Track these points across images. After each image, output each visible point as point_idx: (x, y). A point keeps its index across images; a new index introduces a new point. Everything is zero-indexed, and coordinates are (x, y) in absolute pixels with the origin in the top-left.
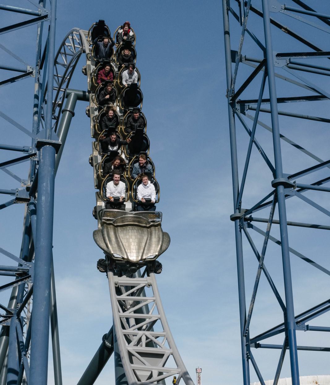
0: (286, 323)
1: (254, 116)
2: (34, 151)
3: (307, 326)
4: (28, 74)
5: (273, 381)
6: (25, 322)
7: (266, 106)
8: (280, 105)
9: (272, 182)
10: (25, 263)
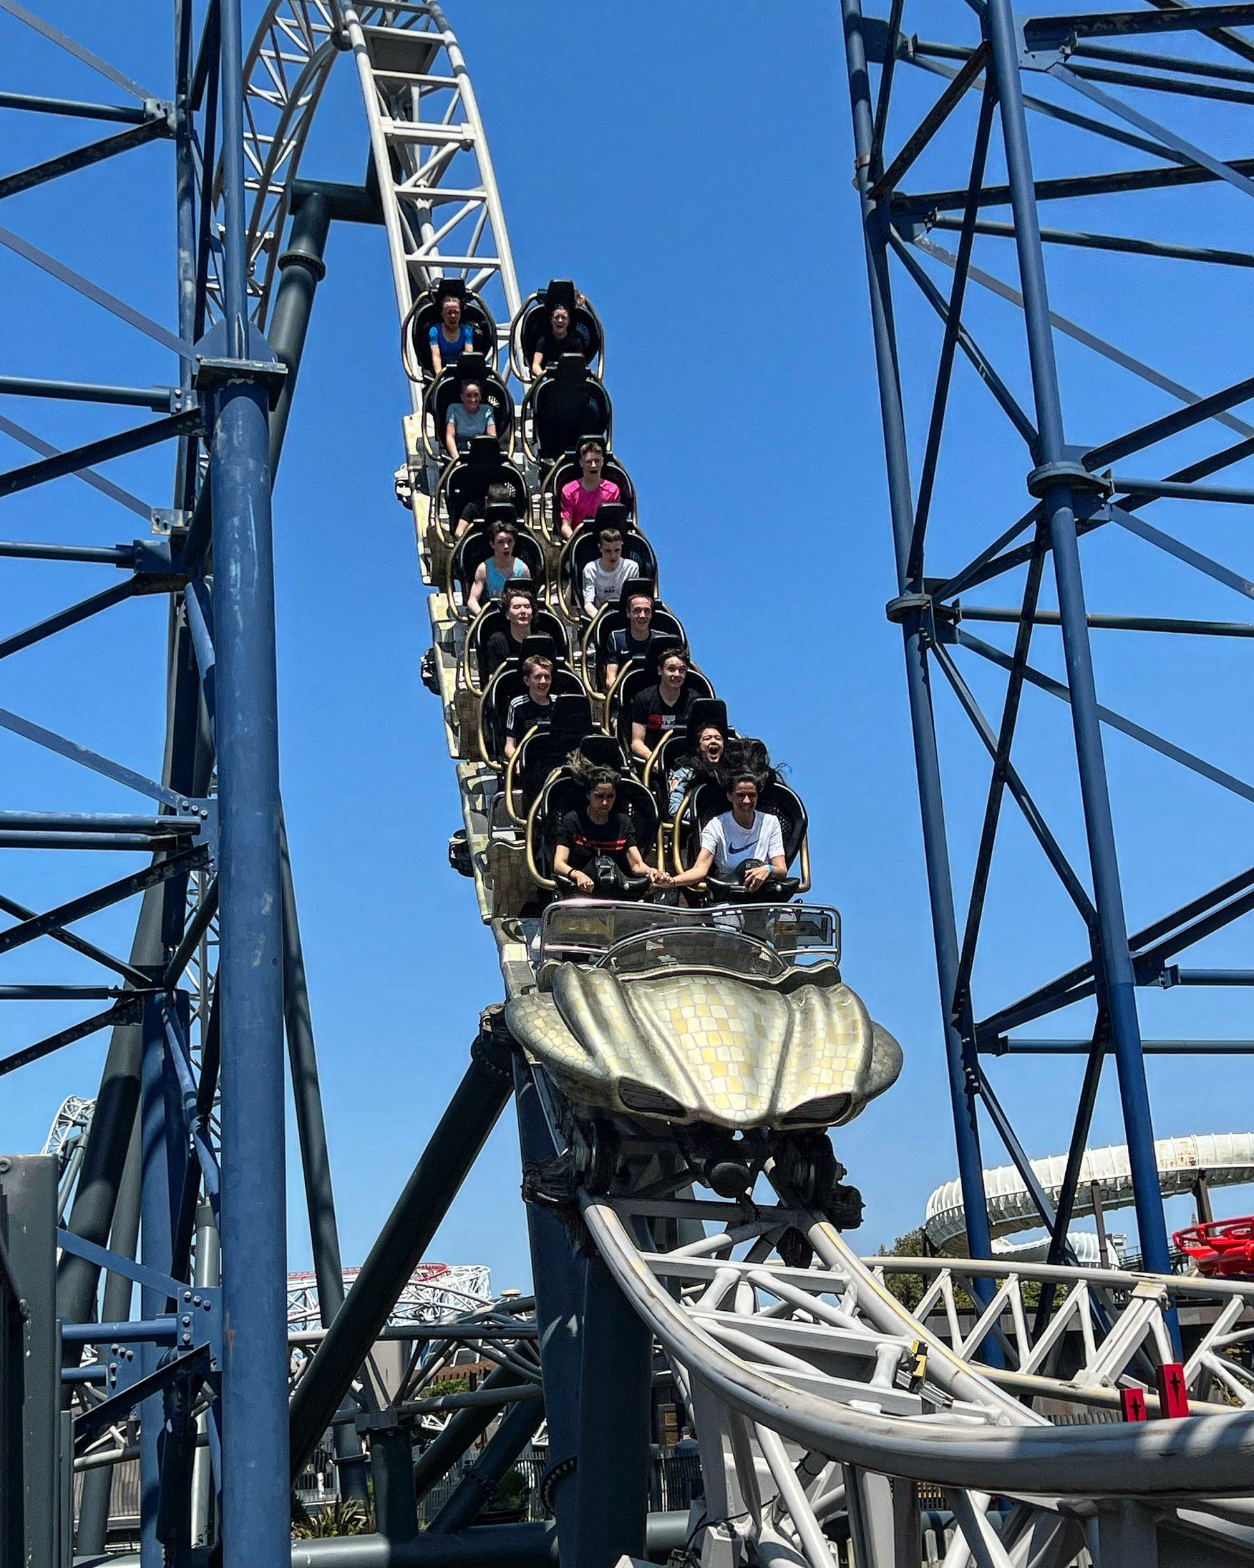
0: (1100, 964)
1: (954, 250)
2: (189, 402)
3: (1175, 968)
4: (158, 128)
5: (1064, 1159)
6: (194, 1010)
7: (998, 215)
8: (1044, 206)
9: (1030, 478)
10: (185, 803)
